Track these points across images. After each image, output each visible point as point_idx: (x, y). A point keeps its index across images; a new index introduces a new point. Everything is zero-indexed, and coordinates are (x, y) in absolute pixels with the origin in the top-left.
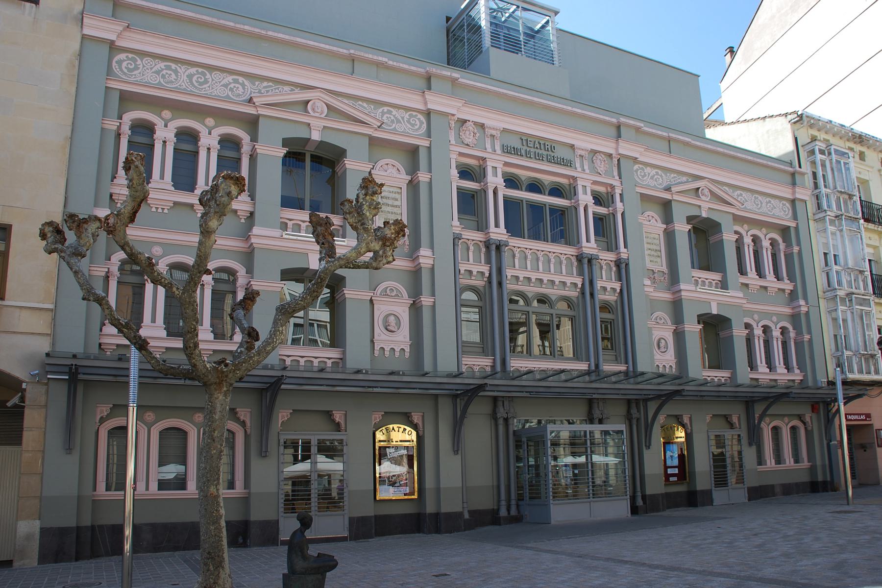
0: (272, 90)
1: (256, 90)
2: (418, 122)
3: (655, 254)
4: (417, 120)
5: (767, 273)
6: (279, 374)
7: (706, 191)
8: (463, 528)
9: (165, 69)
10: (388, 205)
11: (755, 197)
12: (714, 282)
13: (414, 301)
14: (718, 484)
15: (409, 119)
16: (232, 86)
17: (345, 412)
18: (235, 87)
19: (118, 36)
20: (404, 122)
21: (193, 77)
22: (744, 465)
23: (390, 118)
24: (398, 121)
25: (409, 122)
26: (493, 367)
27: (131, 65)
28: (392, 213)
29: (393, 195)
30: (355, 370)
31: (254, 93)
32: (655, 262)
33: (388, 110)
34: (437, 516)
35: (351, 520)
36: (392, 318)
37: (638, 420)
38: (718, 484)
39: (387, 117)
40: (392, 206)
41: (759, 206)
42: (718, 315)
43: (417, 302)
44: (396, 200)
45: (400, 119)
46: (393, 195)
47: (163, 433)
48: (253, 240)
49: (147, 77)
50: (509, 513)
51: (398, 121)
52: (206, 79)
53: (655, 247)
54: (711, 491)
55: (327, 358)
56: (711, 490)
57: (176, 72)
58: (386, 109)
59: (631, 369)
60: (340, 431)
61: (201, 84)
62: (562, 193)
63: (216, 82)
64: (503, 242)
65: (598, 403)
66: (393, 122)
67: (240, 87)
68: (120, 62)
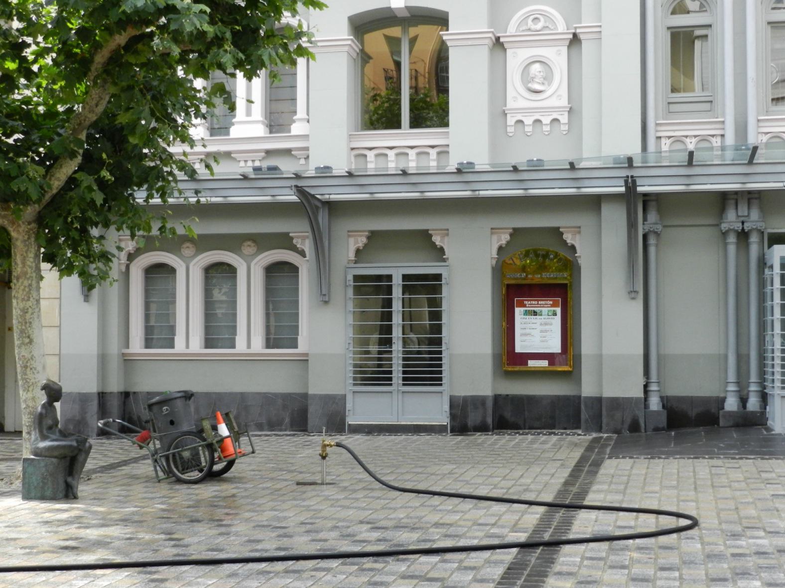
50: (744, 407)
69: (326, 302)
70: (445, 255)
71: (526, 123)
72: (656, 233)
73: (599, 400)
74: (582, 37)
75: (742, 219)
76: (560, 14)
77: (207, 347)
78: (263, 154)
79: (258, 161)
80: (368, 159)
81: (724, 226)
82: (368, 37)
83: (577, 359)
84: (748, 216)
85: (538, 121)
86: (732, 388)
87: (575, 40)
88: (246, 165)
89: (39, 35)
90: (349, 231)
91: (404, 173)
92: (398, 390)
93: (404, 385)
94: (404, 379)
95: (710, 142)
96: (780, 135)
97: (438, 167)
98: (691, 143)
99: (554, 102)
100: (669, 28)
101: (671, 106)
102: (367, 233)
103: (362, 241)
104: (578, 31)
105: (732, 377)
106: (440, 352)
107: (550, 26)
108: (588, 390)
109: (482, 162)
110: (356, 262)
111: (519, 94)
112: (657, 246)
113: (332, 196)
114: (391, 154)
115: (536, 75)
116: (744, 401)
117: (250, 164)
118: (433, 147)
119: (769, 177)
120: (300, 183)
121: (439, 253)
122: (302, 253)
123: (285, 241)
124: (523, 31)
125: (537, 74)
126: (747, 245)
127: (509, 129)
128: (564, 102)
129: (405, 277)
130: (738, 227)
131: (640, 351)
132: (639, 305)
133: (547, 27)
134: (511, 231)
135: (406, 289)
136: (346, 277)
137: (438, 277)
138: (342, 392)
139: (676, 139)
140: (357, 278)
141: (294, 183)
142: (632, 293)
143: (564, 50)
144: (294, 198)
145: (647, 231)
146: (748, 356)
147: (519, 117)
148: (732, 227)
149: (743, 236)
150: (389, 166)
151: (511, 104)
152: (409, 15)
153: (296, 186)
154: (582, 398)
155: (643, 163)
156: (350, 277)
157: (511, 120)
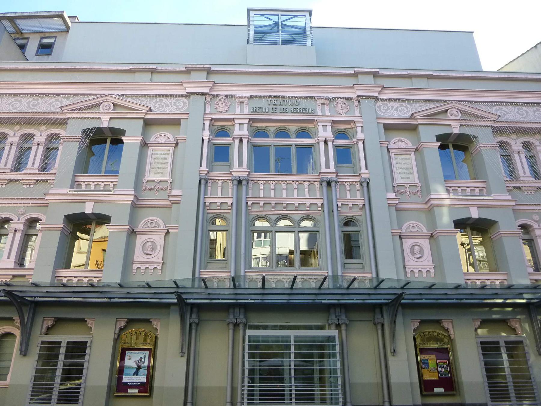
0: (424, 107)
2: (182, 104)
3: (408, 171)
5: (521, 173)
6: (400, 292)
7: (454, 111)
9: (401, 107)
10: (159, 163)
11: (518, 109)
13: (432, 234)
16: (400, 108)
18: (402, 109)
19: (379, 93)
20: (171, 105)
21: (30, 103)
23: (161, 104)
24: (167, 105)
25: (175, 104)
27: (385, 107)
29: (164, 156)
30: (455, 286)
40: (162, 163)
41: (524, 116)
42: (479, 218)
44: (165, 159)
45: (169, 103)
46: (164, 156)
49: (24, 107)
51: (167, 105)
52: (388, 107)
53: (406, 166)
55: (504, 279)
57: (20, 102)
58: (158, 99)
59: (374, 275)
61: (386, 110)
62: (289, 135)
63: (4, 103)
64: (243, 178)
68: (379, 107)
71: (142, 268)
81: (377, 321)
87: (168, 232)
90: (473, 319)
98: (260, 282)
99: (425, 263)
102: (127, 320)
103: (49, 323)
104: (401, 234)
110: (46, 334)
112: (346, 330)
124: (146, 227)
129: (68, 343)
130: (337, 322)
131: (183, 385)
132: (185, 359)
135: (68, 349)
140: (42, 342)
142: (183, 353)
146: (237, 387)
149: (236, 325)
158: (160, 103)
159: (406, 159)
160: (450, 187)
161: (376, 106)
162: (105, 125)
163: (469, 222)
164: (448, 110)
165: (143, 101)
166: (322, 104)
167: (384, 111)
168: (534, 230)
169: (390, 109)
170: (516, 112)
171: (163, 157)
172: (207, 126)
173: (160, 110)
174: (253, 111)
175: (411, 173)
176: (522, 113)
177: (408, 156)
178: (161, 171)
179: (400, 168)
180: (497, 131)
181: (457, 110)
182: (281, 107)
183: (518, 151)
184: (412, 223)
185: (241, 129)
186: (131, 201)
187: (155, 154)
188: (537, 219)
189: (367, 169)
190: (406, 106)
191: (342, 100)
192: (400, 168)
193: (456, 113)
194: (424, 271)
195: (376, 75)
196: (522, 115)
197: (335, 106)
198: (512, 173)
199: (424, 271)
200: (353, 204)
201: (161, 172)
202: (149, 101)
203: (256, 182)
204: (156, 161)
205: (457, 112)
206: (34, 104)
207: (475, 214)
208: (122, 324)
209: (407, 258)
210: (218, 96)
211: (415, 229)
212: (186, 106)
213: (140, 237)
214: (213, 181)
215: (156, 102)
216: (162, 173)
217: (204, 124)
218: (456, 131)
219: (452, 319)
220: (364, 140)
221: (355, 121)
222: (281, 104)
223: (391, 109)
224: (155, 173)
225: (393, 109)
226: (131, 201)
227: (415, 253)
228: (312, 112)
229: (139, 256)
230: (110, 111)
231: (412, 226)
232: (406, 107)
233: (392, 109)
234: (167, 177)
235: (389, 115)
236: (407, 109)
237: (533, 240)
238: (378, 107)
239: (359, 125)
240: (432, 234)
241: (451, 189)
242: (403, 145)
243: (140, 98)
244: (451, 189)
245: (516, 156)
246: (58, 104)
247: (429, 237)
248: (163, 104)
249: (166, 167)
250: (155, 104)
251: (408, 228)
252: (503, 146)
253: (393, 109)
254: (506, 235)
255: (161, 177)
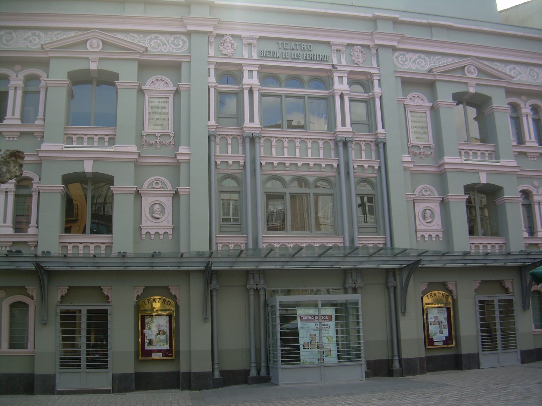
1: (48, 38)
2: (181, 43)
3: (422, 131)
4: (180, 41)
5: (527, 138)
7: (472, 68)
8: (212, 386)
12: (487, 153)
14: (91, 365)
15: (174, 41)
17: (455, 283)
18: (420, 61)
20: (169, 44)
22: (516, 329)
23: (157, 42)
24: (164, 44)
25: (173, 43)
26: (385, 244)
28: (161, 120)
29: (162, 105)
31: (47, 41)
32: (422, 138)
33: (155, 36)
34: (189, 374)
35: (114, 376)
36: (157, 207)
37: (395, 288)
38: (91, 365)
39: (154, 42)
40: (161, 114)
41: (535, 77)
42: (487, 184)
43: (445, 198)
44: (165, 108)
45: (166, 42)
46: (162, 105)
47: (13, 306)
48: (178, 158)
50: (259, 374)
51: (164, 44)
53: (421, 125)
54: (478, 355)
56: (478, 354)
58: (153, 36)
60: (508, 294)
61: (404, 62)
65: (352, 273)
66: (159, 45)
67: (37, 38)
69: (45, 324)
70: (109, 300)
71: (433, 236)
72: (217, 290)
73: (189, 374)
74: (180, 193)
75: (256, 283)
76: (167, 179)
77: (10, 348)
78: (12, 243)
79: (8, 247)
80: (69, 249)
82: (71, 186)
83: (178, 353)
84: (259, 282)
85: (148, 233)
86: (253, 365)
88: (2, 249)
89: (23, 175)
90: (134, 286)
91: (65, 256)
92: (84, 371)
93: (87, 368)
94: (87, 365)
95: (240, 246)
96: (285, 244)
97: (106, 254)
100: (265, 193)
101: (222, 228)
103: (64, 291)
105: (253, 359)
106: (107, 351)
107: (164, 187)
108: (183, 368)
109: (130, 251)
111: (149, 219)
113: (50, 267)
114: (481, 246)
115: (157, 210)
116: (259, 371)
117: (4, 248)
118: (103, 243)
119: (246, 264)
120: (38, 260)
121: (107, 299)
122: (32, 298)
123: (22, 290)
124: (150, 188)
125: (157, 209)
126: (259, 296)
127: (142, 236)
128: (170, 224)
129: (88, 311)
130: (255, 287)
133: (162, 187)
134: (68, 288)
135: (88, 318)
136: (56, 311)
137: (106, 311)
138: (53, 373)
139: (282, 244)
141: (34, 260)
142: (205, 319)
143: (171, 199)
144: (33, 268)
145: (212, 288)
147: (148, 230)
148: (252, 287)
149: (257, 291)
150: (68, 253)
151: (144, 223)
152: (92, 177)
153: (35, 262)
154: (181, 373)
155: (105, 255)
156: (58, 311)
157: (144, 232)
158: (155, 41)
159: (421, 117)
160: (463, 150)
161: (394, 56)
162: (94, 66)
163: (477, 186)
164: (465, 66)
165: (136, 38)
166: (337, 50)
167: (401, 63)
168: (533, 196)
169: (408, 60)
170: (528, 73)
171: (162, 106)
172: (212, 72)
173: (157, 49)
174: (262, 55)
175: (426, 133)
176: (533, 74)
177: (423, 114)
178: (161, 122)
179: (416, 127)
180: (510, 92)
181: (474, 68)
182: (293, 52)
183: (527, 114)
184: (425, 187)
185: (251, 77)
186: (135, 159)
187: (152, 102)
188: (536, 185)
189: (383, 128)
190: (425, 58)
191: (359, 47)
192: (416, 127)
193: (473, 71)
194: (434, 235)
195: (395, 22)
196: (533, 76)
197: (352, 53)
198: (520, 140)
199: (434, 235)
200: (369, 166)
201: (161, 123)
202: (143, 37)
203: (268, 138)
204: (154, 110)
205: (474, 69)
206: (8, 39)
207: (483, 179)
208: (140, 291)
209: (418, 223)
210: (223, 36)
211: (427, 193)
212: (185, 46)
213: (146, 199)
214: (221, 136)
215: (151, 39)
216: (162, 125)
217: (209, 69)
218: (472, 90)
219: (111, 286)
220: (381, 95)
221: (372, 73)
222: (293, 48)
223: (409, 60)
224: (155, 125)
225: (411, 62)
226: (135, 159)
227: (426, 217)
228: (324, 59)
229: (146, 221)
230: (98, 50)
231: (424, 189)
232: (424, 59)
233: (410, 61)
234: (170, 130)
235: (407, 67)
236: (425, 62)
237: (531, 205)
238: (395, 58)
239: (376, 78)
240: (443, 198)
241: (463, 152)
242: (418, 102)
243: (132, 34)
244: (463, 152)
245: (524, 119)
246: (35, 39)
247: (439, 202)
248: (159, 43)
249: (166, 118)
250: (150, 42)
251: (421, 191)
252: (515, 107)
253: (411, 62)
254: (509, 201)
255: (162, 130)
